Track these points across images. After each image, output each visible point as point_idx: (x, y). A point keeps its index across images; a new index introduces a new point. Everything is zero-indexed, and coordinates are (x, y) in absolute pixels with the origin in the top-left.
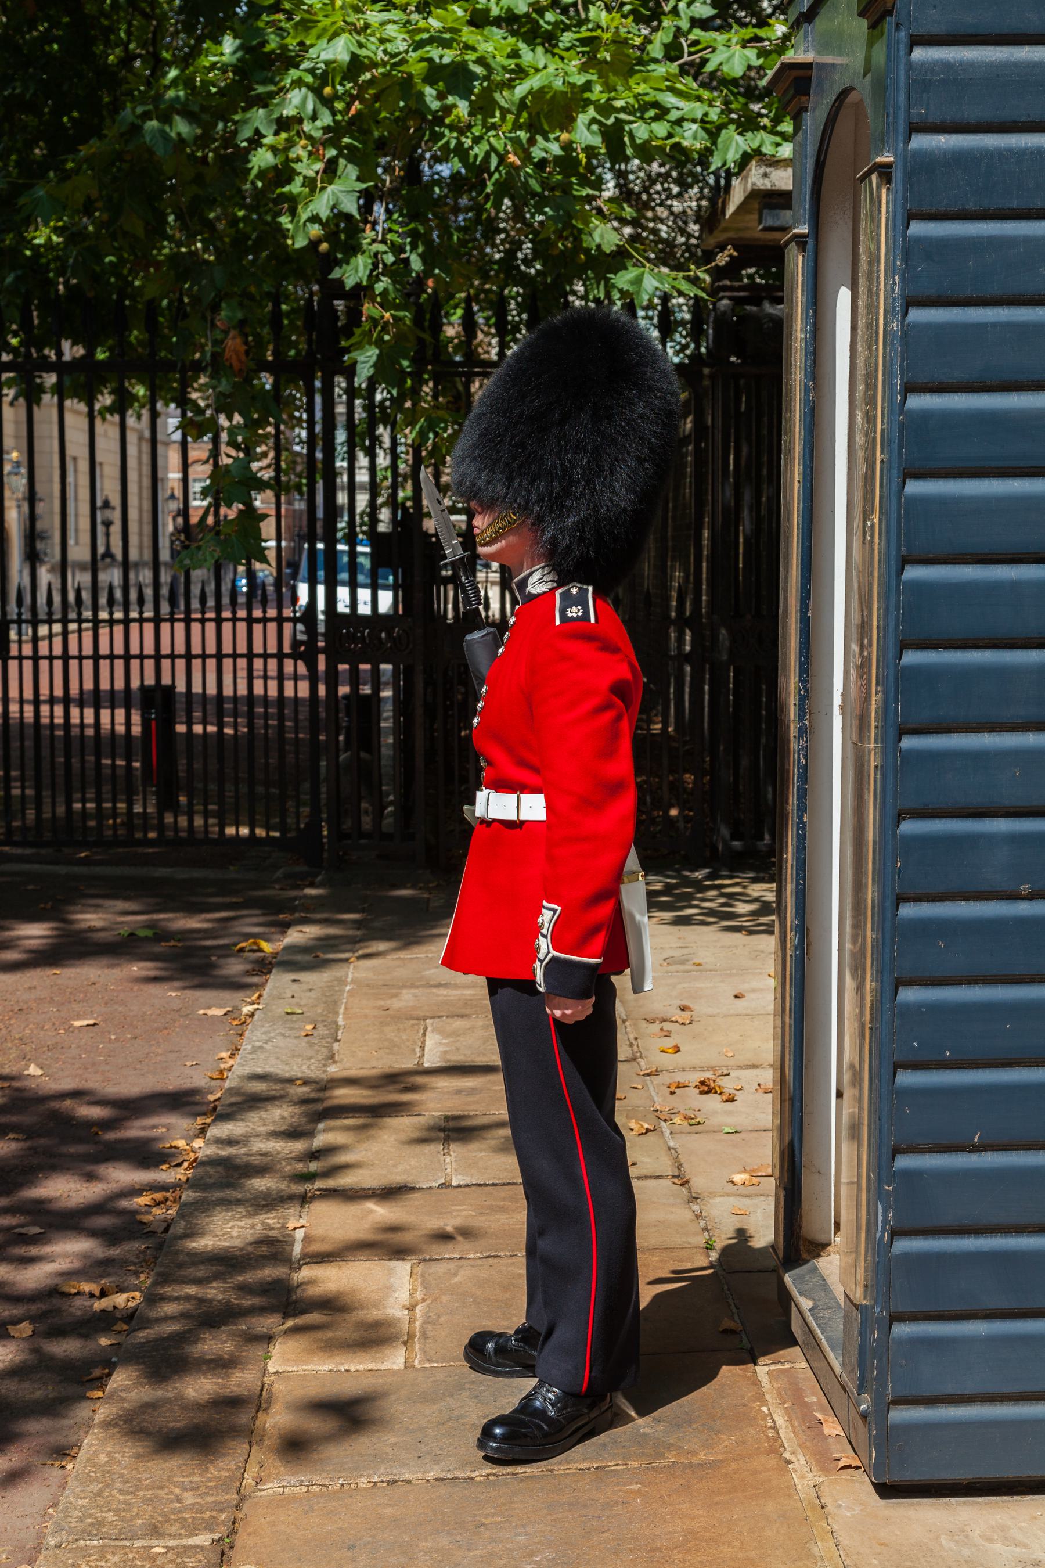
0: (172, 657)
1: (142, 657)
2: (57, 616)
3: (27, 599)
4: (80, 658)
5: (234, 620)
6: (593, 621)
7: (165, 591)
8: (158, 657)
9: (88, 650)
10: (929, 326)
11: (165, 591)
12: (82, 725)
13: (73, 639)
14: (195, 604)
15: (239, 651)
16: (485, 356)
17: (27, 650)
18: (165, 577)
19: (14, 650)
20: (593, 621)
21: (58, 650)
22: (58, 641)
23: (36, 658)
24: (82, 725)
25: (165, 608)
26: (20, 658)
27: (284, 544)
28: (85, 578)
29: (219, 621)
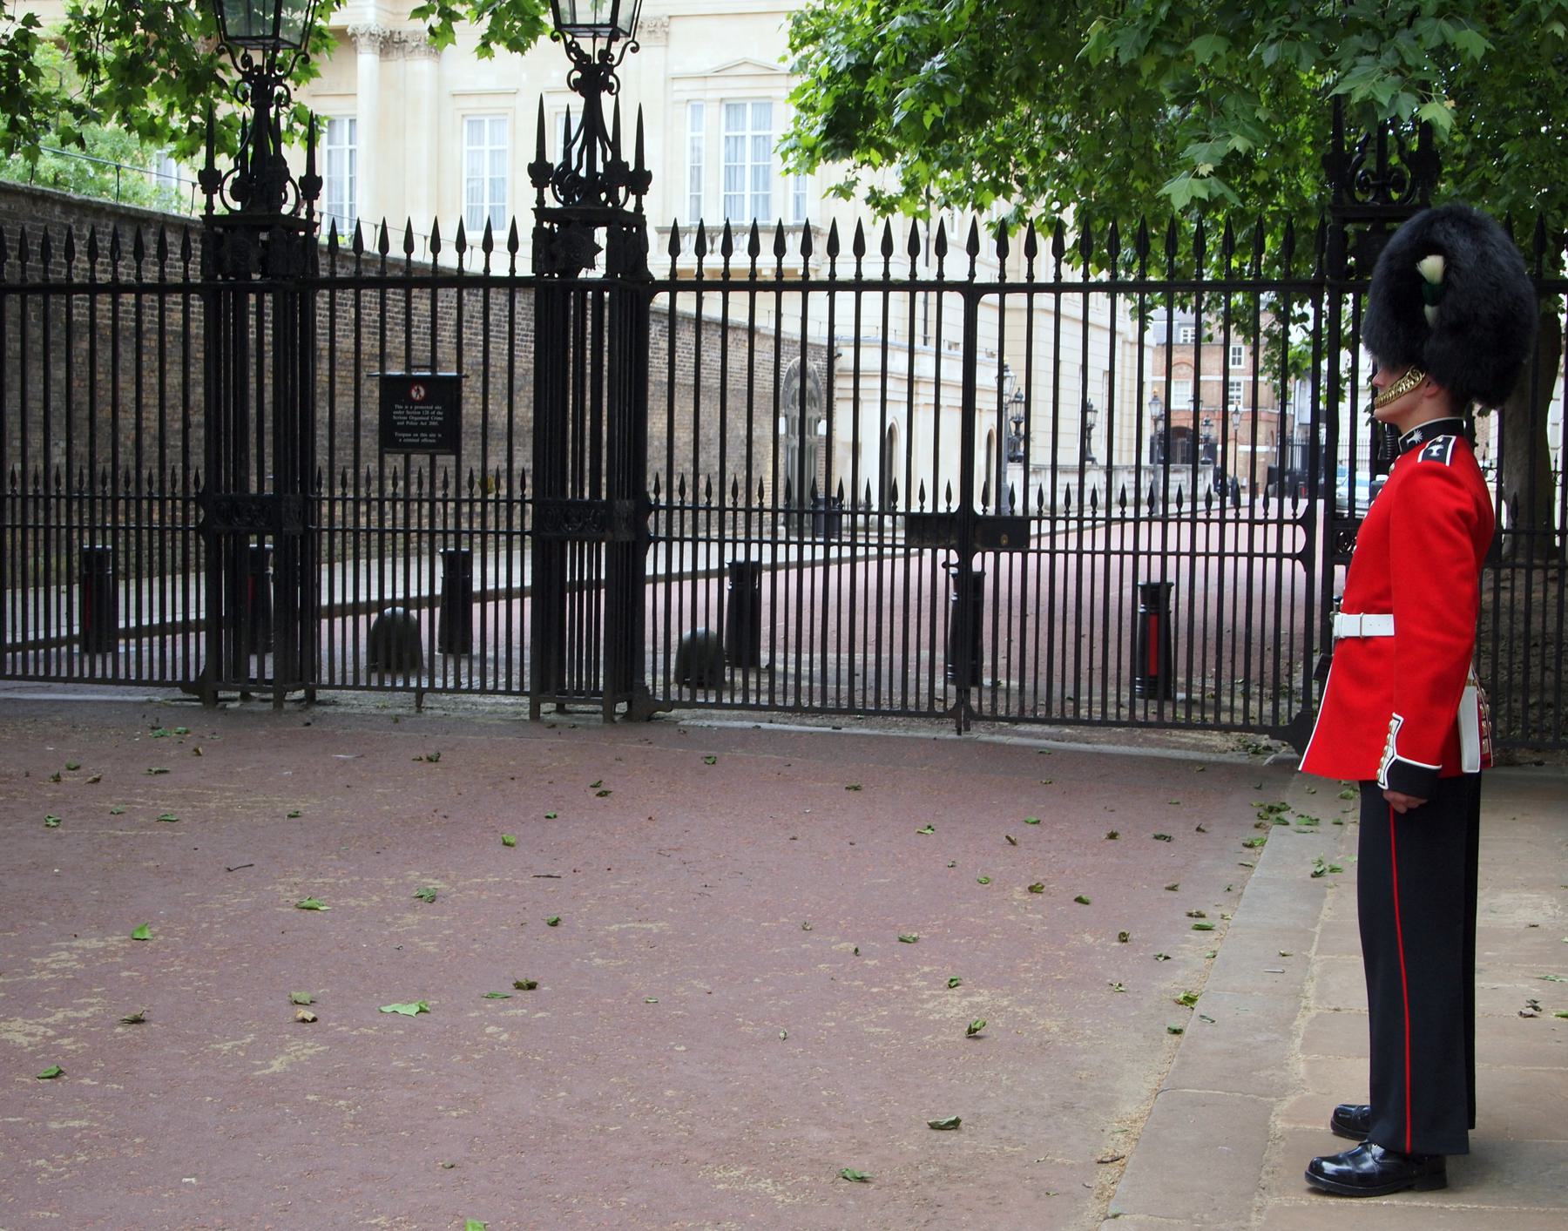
0: (1178, 554)
1: (1149, 554)
2: (1074, 515)
3: (1047, 500)
4: (1093, 553)
5: (1237, 521)
6: (604, 497)
7: (1145, 495)
8: (1164, 554)
9: (1100, 546)
10: (80, 625)
11: (1145, 495)
12: (814, 544)
13: (1087, 535)
14: (1201, 505)
15: (1240, 550)
16: (1215, 294)
17: (1045, 545)
18: (1145, 483)
19: (1033, 545)
20: (604, 497)
21: (1073, 546)
22: (1073, 537)
23: (1053, 553)
24: (814, 544)
25: (1144, 511)
26: (1039, 552)
27: (1259, 449)
28: (1074, 480)
29: (1222, 522)
